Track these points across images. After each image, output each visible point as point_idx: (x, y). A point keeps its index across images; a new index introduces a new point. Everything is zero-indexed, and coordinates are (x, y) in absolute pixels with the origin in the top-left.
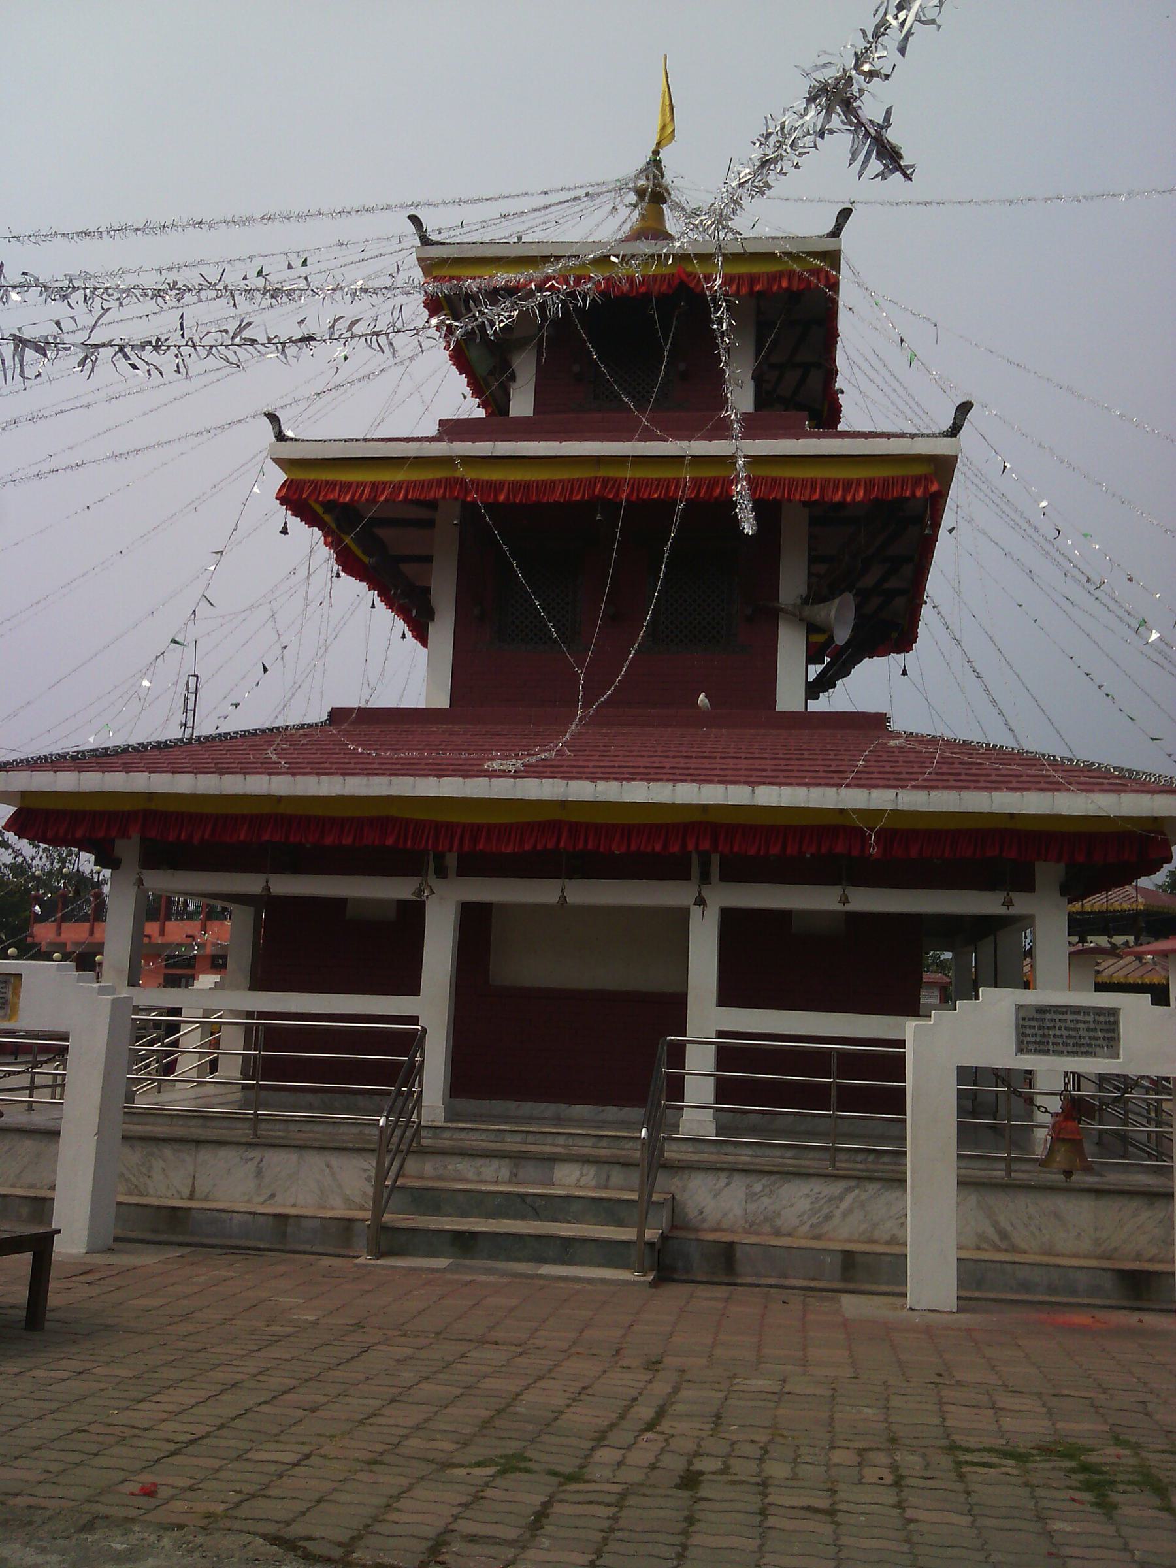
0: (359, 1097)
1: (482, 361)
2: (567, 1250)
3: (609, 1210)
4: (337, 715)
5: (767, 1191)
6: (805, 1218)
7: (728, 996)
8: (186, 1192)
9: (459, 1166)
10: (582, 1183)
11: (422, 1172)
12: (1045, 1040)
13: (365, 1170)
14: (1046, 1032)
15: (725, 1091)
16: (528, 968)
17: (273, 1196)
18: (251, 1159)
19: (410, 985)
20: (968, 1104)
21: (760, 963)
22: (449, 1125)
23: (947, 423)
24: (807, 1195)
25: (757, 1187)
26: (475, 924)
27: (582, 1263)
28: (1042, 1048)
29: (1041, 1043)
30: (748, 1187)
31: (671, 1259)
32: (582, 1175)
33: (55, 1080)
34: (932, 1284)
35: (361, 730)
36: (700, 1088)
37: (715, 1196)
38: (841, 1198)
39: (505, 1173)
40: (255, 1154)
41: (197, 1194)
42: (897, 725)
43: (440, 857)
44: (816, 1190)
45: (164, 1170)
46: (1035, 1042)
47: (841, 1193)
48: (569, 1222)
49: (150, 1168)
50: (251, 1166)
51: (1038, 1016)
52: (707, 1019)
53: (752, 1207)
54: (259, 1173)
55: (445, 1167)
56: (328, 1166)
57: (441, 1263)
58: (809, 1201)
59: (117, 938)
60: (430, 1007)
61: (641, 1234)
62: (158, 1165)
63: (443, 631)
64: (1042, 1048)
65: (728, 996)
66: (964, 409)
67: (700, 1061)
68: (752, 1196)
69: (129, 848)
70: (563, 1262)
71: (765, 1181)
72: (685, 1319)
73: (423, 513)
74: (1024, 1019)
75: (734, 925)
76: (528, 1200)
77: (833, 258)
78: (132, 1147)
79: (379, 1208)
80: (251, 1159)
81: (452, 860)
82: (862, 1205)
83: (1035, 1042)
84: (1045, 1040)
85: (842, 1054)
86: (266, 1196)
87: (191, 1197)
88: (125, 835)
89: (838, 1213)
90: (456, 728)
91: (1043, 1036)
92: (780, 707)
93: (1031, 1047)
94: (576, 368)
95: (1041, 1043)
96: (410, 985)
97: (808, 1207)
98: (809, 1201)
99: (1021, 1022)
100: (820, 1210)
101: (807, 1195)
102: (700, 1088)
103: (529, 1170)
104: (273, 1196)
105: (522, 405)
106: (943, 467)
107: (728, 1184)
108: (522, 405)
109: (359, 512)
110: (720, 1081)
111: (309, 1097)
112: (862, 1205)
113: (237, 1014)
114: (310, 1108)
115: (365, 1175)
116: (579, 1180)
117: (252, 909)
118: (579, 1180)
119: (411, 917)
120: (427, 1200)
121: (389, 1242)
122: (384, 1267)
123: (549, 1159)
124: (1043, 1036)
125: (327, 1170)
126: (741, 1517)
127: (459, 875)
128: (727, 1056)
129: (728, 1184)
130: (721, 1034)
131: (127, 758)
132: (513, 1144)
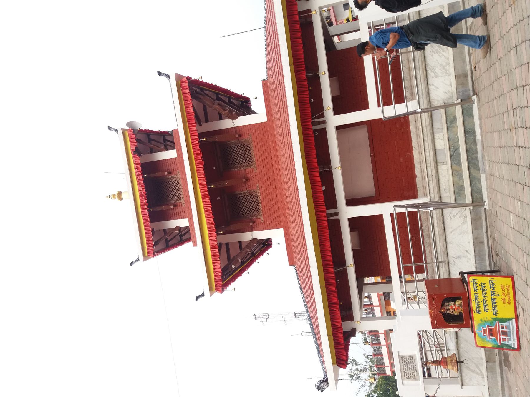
0: (424, 234)
1: (183, 236)
2: (469, 132)
3: (451, 122)
6: (441, 55)
7: (365, 106)
9: (444, 184)
10: (442, 138)
11: (448, 197)
13: (451, 219)
15: (400, 99)
16: (367, 184)
17: (467, 251)
19: (379, 218)
21: (350, 97)
22: (429, 196)
23: (165, 78)
24: (432, 56)
25: (432, 74)
26: (350, 202)
27: (474, 125)
30: (433, 77)
32: (439, 138)
33: (438, 351)
35: (295, 256)
36: (400, 109)
37: (438, 88)
39: (444, 167)
40: (451, 260)
42: (265, 78)
43: (332, 215)
44: (430, 53)
48: (458, 137)
50: (457, 261)
52: (375, 111)
53: (440, 75)
54: (459, 258)
55: (445, 189)
57: (483, 177)
58: (434, 55)
59: (381, 325)
60: (385, 210)
61: (457, 104)
65: (365, 106)
67: (391, 111)
68: (436, 76)
69: (347, 326)
70: (474, 132)
71: (429, 72)
73: (224, 249)
75: (337, 111)
76: (452, 153)
77: (124, 131)
79: (465, 205)
85: (403, 264)
86: (467, 254)
88: (341, 327)
90: (289, 222)
92: (266, 120)
96: (379, 218)
97: (436, 54)
98: (434, 55)
100: (437, 50)
101: (432, 56)
102: (400, 109)
103: (440, 158)
104: (467, 251)
105: (183, 223)
106: (179, 78)
107: (433, 85)
109: (230, 265)
111: (427, 252)
113: (401, 286)
114: (430, 251)
117: (364, 286)
119: (353, 222)
120: (459, 190)
121: (477, 201)
122: (490, 199)
123: (435, 152)
128: (387, 102)
129: (433, 85)
130: (379, 106)
131: (315, 330)
132: (431, 170)
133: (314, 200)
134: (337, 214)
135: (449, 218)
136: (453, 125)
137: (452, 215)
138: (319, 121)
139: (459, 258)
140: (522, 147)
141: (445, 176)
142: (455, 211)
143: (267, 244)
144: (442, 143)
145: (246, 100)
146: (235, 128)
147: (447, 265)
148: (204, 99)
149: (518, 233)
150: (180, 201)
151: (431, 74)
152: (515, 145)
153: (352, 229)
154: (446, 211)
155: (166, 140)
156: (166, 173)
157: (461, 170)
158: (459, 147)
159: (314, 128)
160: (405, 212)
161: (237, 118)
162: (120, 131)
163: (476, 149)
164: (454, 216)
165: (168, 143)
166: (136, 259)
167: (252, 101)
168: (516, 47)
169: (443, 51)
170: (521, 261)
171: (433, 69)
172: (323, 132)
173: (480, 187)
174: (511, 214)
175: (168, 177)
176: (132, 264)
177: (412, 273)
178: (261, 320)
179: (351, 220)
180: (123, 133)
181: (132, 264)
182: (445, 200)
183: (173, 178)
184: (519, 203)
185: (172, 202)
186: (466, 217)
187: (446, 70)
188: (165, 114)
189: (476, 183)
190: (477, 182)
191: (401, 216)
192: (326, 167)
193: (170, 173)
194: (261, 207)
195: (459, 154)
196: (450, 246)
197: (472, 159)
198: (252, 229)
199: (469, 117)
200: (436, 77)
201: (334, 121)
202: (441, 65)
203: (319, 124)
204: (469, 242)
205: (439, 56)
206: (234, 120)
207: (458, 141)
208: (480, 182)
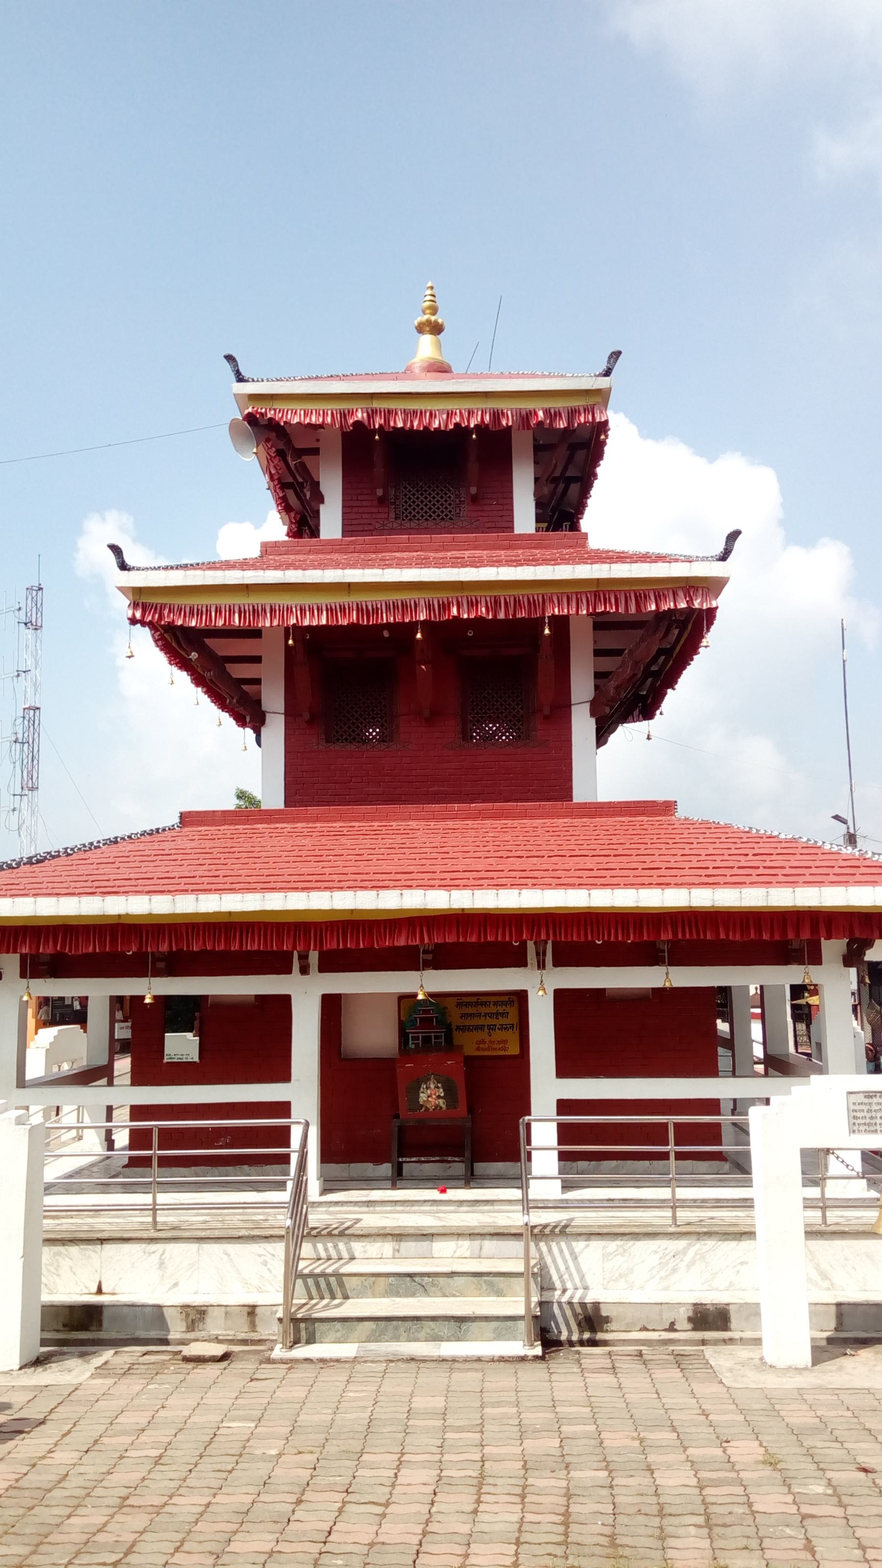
2: (460, 1324)
4: (187, 819)
5: (621, 1250)
7: (566, 1067)
8: (94, 1289)
10: (457, 1255)
12: (873, 1122)
13: (260, 1256)
14: (874, 1114)
15: (566, 1134)
17: (176, 1285)
18: (154, 1252)
19: (283, 1075)
20: (713, 1134)
21: (594, 1035)
23: (603, 366)
24: (656, 1252)
26: (332, 1008)
28: (872, 1128)
29: (869, 1124)
31: (565, 1331)
32: (457, 1247)
34: (787, 1335)
36: (544, 1134)
38: (684, 1251)
41: (104, 1289)
42: (682, 812)
43: (304, 957)
45: (71, 1268)
46: (865, 1124)
47: (684, 1248)
49: (58, 1267)
50: (155, 1258)
51: (866, 1101)
54: (162, 1264)
56: (226, 1254)
62: (65, 1263)
63: (275, 729)
64: (872, 1128)
66: (733, 536)
68: (606, 1257)
72: (573, 1380)
74: (854, 1104)
78: (174, 896)
79: (289, 1293)
80: (154, 1252)
81: (314, 957)
82: (703, 1258)
83: (865, 1124)
84: (873, 1122)
87: (99, 1291)
89: (682, 1265)
91: (872, 1118)
93: (862, 1128)
94: (380, 492)
95: (869, 1124)
96: (283, 1075)
99: (852, 1107)
100: (667, 1263)
101: (656, 1252)
102: (544, 1134)
103: (410, 1247)
104: (176, 1285)
105: (331, 522)
108: (331, 522)
110: (561, 1127)
112: (703, 1258)
115: (261, 1260)
116: (455, 1252)
118: (455, 1252)
119: (279, 1009)
124: (872, 1118)
125: (226, 1257)
126: (377, 1450)
127: (321, 970)
133: (348, 921)
134: (304, 970)
135: (262, 1252)
136: (484, 1287)
137: (268, 1258)
138: (544, 954)
139: (162, 1264)
140: (391, 1494)
141: (365, 1252)
142: (278, 1269)
143: (247, 711)
144: (447, 1256)
145: (646, 707)
146: (569, 706)
147: (145, 1235)
148: (652, 641)
149: (208, 1438)
150: (392, 515)
151: (613, 1245)
152: (406, 1458)
153: (263, 1000)
154: (279, 1249)
155: (562, 510)
156: (473, 490)
157: (374, 1296)
158: (429, 1296)
159: (531, 945)
160: (289, 1147)
161: (592, 714)
162: (603, 383)
163: (417, 1340)
164: (265, 1263)
165: (562, 486)
166: (244, 373)
167: (642, 726)
168: (611, 1487)
169: (661, 1278)
170: (143, 1438)
171: (625, 1250)
172: (518, 960)
173: (327, 1340)
174: (253, 1425)
175: (463, 491)
176: (230, 358)
177: (132, 1146)
178: (23, 606)
179: (284, 1003)
180: (598, 392)
181: (230, 358)
182: (307, 1249)
183: (458, 506)
184: (274, 1452)
185: (392, 492)
186: (259, 1290)
187: (616, 1280)
188: (642, 512)
189: (338, 1331)
190: (339, 1334)
191: (282, 1136)
192: (429, 957)
193: (475, 499)
194: (348, 747)
195: (413, 1295)
196: (194, 1247)
197: (396, 1328)
198: (291, 714)
199: (496, 1329)
200: (603, 1255)
201: (540, 989)
202: (631, 1270)
203: (538, 954)
204: (196, 1293)
205: (653, 1268)
206: (588, 706)
207: (445, 1296)
208: (338, 1341)
